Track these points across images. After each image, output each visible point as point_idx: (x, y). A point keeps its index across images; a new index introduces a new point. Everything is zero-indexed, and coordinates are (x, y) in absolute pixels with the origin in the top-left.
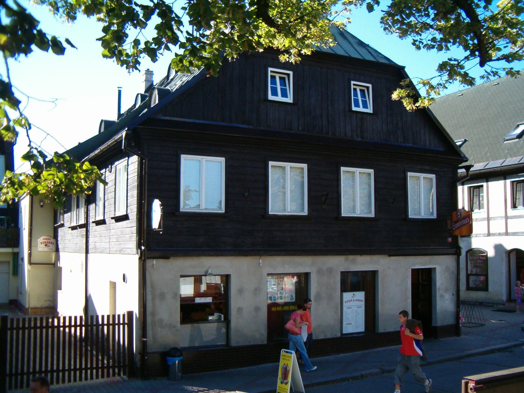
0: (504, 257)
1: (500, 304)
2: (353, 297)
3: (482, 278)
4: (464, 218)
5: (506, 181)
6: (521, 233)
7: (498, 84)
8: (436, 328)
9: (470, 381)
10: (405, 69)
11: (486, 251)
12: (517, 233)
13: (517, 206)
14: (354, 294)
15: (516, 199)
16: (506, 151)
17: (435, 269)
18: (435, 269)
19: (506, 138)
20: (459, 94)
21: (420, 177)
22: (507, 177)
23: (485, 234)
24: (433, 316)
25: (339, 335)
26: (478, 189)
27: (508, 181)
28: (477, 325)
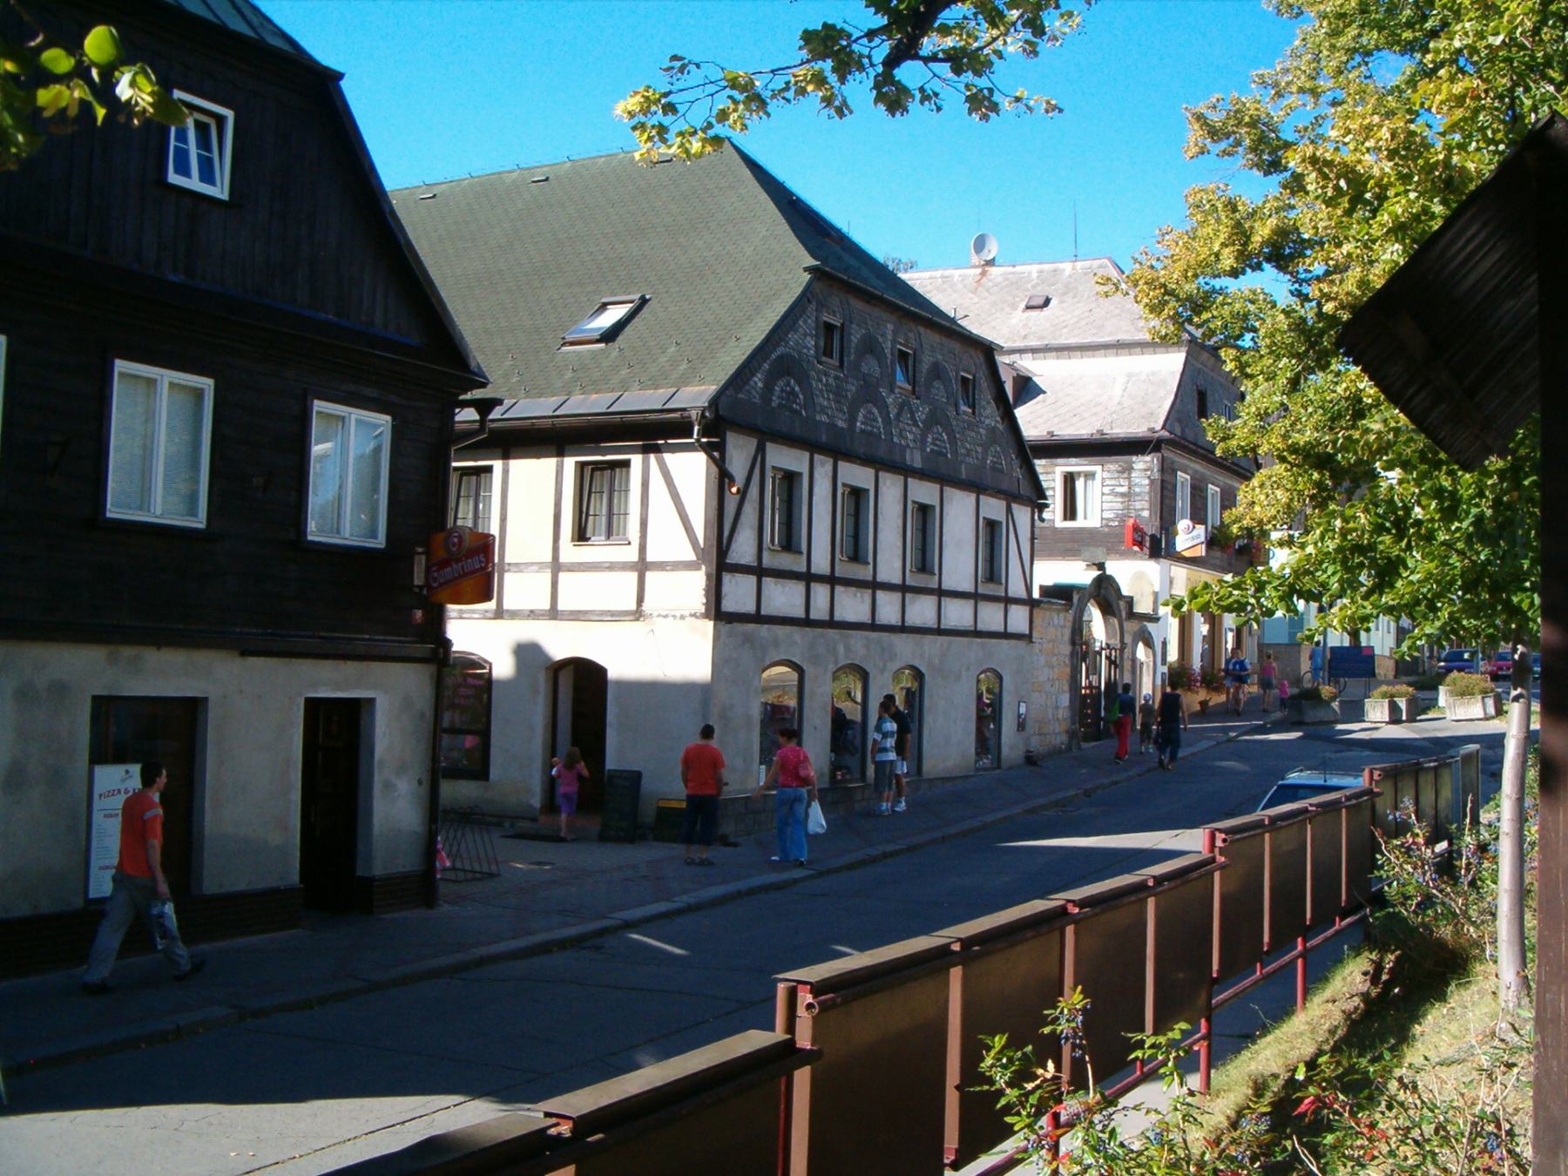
0: (542, 680)
1: (523, 818)
2: (123, 780)
3: (470, 741)
4: (472, 553)
5: (562, 463)
6: (598, 615)
7: (547, 179)
8: (370, 881)
9: (800, 986)
10: (344, 84)
11: (486, 661)
12: (586, 612)
13: (588, 536)
14: (127, 772)
15: (587, 515)
16: (569, 375)
17: (371, 701)
18: (371, 701)
19: (569, 338)
20: (423, 194)
21: (347, 419)
22: (567, 448)
23: (486, 611)
24: (360, 847)
25: (79, 903)
26: (475, 477)
27: (570, 463)
28: (478, 875)
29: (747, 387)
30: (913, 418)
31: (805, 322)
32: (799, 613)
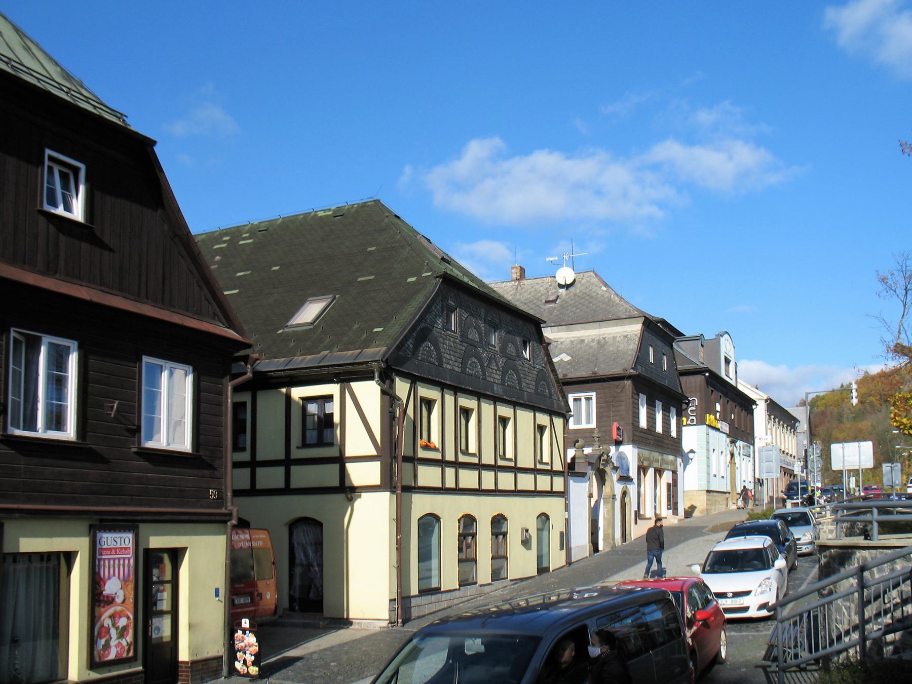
10: (156, 149)
29: (404, 348)
30: (497, 365)
31: (436, 307)
32: (475, 486)
